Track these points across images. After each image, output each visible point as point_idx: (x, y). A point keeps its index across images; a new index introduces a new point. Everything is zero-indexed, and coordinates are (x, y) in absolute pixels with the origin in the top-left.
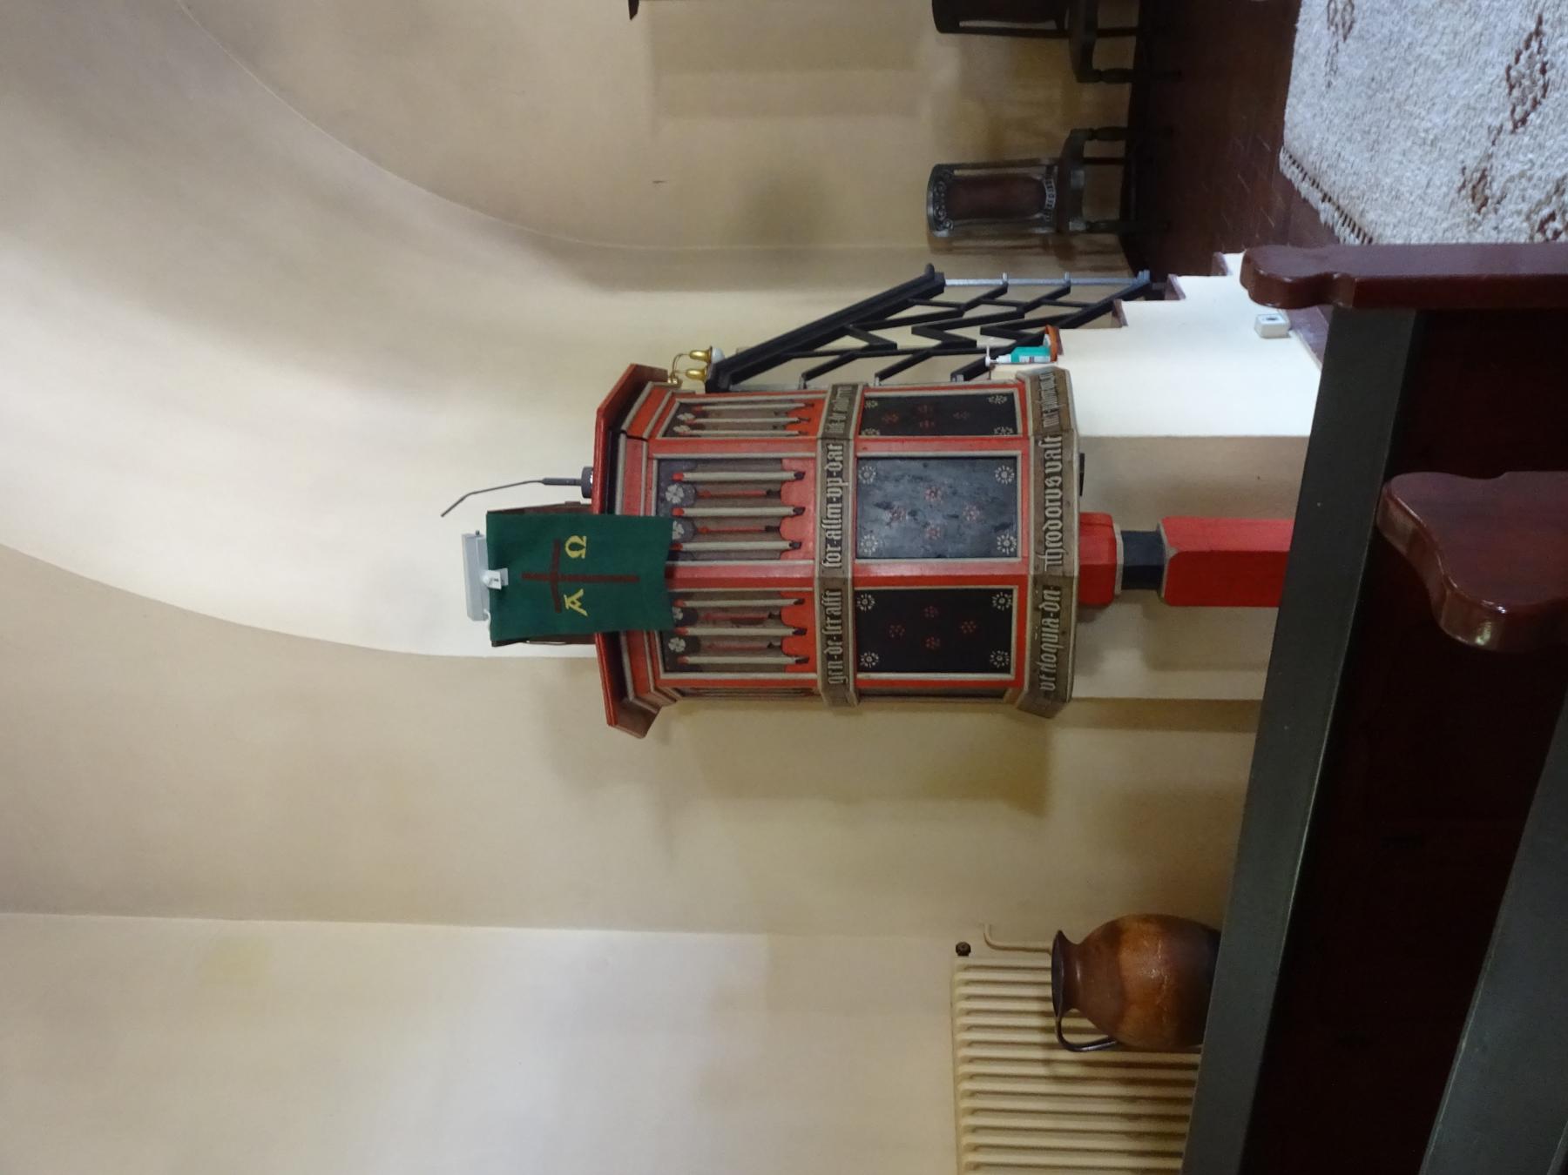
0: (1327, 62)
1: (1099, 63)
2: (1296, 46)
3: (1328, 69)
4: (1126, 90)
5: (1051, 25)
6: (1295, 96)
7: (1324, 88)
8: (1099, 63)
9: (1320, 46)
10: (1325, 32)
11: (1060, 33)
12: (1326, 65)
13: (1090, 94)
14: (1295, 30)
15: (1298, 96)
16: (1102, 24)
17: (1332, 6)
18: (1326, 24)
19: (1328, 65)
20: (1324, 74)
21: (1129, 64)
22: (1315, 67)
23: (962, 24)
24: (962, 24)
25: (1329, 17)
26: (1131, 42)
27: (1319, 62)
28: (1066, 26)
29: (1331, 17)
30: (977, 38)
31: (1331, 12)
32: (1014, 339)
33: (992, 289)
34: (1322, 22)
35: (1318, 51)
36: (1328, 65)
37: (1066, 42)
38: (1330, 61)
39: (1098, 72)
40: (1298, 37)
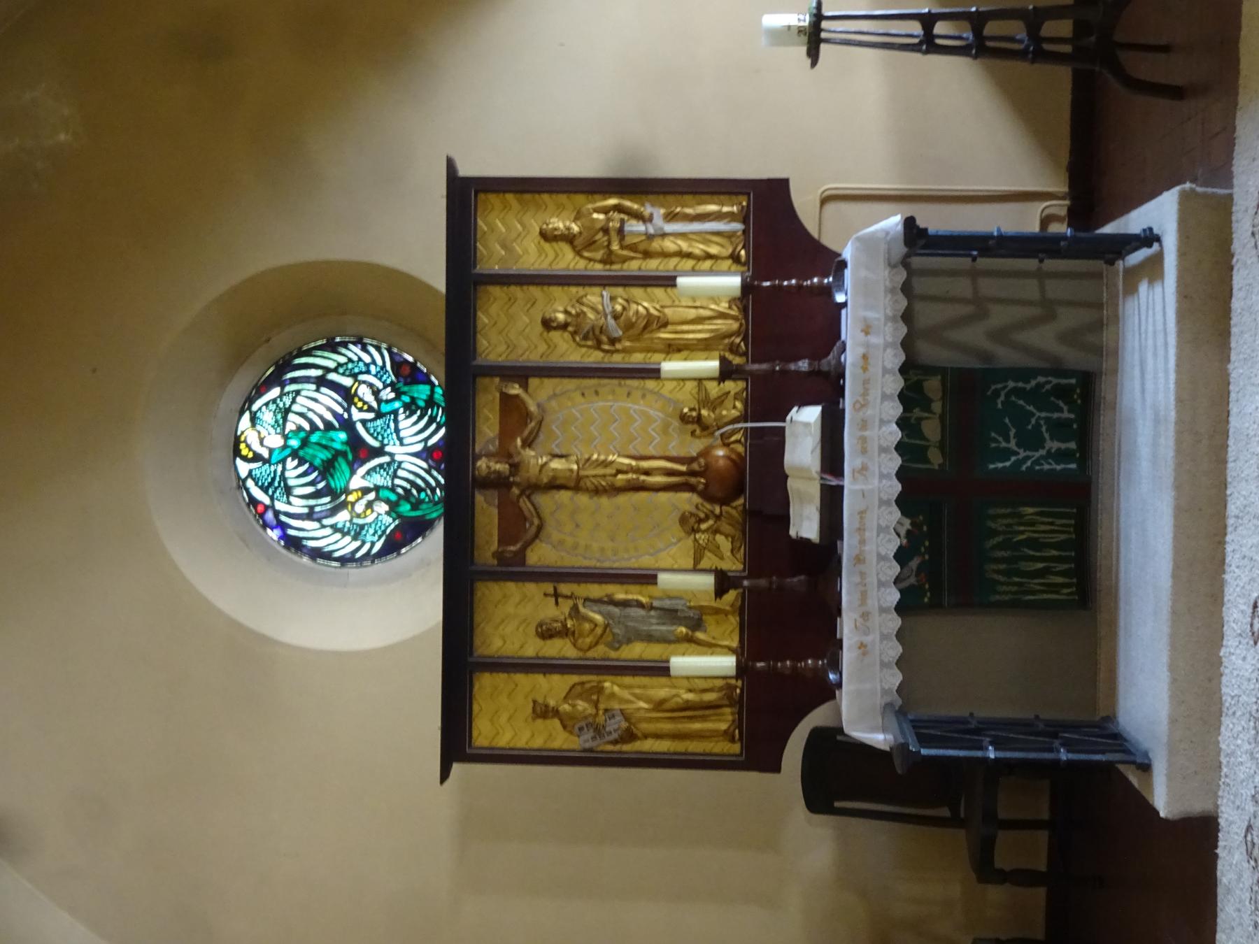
0: (1251, 898)
1: (1002, 861)
2: (1219, 874)
3: (1253, 908)
4: (1041, 893)
5: (945, 812)
6: (1224, 932)
7: (1251, 929)
8: (1002, 861)
9: (1243, 880)
10: (1245, 865)
11: (954, 822)
12: (1250, 903)
13: (996, 894)
14: (1216, 856)
15: (1227, 931)
16: (1002, 814)
17: (1249, 838)
18: (1246, 857)
19: (1252, 902)
20: (1249, 913)
21: (1045, 815)
22: (1240, 902)
23: (837, 804)
24: (837, 804)
25: (1247, 850)
26: (1043, 836)
27: (1243, 897)
28: (962, 815)
29: (1249, 850)
30: (854, 821)
31: (1249, 844)
32: (294, 365)
33: (619, 679)
34: (1241, 853)
35: (1241, 885)
36: (1252, 902)
37: (961, 834)
38: (1253, 898)
39: (1001, 871)
40: (1220, 865)
